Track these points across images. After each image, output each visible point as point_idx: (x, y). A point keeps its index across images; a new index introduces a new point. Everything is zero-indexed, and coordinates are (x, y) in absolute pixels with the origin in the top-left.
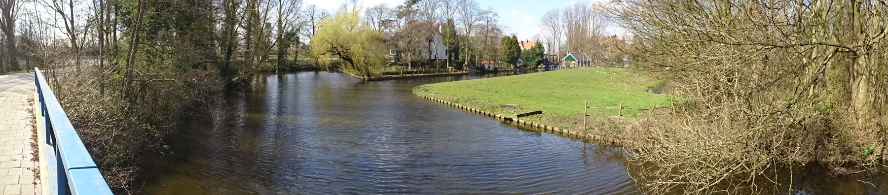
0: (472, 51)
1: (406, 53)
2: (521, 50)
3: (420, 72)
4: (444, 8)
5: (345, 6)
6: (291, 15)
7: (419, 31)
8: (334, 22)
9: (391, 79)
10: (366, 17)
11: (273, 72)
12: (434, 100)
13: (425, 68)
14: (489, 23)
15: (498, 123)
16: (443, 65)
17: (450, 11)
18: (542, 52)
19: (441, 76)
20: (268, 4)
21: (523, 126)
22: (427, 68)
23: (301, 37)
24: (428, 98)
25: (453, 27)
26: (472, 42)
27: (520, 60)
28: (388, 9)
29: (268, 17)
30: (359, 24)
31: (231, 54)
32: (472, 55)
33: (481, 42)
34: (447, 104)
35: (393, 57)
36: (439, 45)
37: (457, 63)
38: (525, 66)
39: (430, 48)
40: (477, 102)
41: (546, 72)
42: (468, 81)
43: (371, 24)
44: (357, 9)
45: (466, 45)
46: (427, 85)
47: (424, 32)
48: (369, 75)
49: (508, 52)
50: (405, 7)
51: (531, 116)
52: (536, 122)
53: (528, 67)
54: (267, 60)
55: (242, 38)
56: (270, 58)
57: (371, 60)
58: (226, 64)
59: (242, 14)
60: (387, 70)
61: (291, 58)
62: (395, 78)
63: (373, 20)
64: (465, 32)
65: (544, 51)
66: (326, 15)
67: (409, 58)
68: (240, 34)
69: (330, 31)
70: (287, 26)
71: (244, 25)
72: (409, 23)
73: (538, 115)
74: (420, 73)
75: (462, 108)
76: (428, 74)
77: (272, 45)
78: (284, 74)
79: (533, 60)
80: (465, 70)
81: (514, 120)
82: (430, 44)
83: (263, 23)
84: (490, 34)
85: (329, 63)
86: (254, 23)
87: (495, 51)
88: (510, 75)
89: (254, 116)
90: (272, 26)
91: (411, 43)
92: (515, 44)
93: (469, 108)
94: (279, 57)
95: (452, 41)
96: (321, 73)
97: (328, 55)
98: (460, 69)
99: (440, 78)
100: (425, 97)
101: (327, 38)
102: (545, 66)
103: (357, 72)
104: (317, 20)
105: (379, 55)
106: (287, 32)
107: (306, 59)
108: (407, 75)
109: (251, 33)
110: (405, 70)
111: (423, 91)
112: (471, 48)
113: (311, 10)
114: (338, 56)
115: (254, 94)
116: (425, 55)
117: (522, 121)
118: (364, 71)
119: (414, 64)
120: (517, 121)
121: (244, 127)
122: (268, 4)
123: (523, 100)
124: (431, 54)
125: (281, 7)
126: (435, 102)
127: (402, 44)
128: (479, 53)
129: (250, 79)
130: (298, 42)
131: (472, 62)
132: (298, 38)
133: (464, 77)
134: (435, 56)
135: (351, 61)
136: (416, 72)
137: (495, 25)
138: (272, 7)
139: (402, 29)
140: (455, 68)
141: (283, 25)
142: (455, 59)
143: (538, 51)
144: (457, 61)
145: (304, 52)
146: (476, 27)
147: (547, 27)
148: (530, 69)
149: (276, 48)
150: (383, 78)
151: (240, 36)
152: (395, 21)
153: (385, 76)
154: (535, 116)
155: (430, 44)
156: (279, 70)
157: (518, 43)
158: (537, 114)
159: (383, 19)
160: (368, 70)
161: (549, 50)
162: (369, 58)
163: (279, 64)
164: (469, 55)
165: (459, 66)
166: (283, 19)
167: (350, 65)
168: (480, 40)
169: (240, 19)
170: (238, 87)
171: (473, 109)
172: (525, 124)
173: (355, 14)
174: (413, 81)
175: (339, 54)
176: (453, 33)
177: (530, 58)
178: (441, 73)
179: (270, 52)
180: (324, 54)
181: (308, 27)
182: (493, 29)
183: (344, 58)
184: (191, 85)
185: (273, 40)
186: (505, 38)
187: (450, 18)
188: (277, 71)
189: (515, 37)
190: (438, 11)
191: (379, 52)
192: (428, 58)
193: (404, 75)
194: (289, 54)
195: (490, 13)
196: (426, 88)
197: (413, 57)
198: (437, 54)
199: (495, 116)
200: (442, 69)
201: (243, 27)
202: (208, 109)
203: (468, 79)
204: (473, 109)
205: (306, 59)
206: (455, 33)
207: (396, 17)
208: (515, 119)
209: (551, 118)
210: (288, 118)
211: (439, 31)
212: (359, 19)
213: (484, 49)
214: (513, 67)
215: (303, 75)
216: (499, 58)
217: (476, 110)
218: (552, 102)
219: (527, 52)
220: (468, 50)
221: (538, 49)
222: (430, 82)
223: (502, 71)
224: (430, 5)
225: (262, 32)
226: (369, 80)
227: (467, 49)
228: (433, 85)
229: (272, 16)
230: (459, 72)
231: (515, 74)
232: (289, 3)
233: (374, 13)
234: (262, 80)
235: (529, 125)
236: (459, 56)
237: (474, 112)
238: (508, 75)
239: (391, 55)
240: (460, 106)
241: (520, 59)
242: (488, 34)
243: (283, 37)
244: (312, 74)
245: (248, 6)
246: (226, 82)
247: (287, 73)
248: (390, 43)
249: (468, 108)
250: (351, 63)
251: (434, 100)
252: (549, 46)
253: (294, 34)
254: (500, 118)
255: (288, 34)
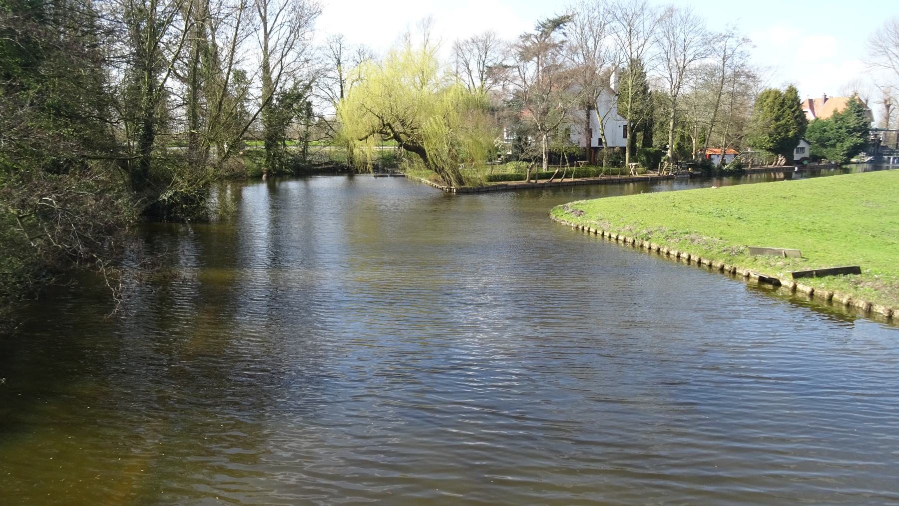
0: (683, 127)
1: (538, 133)
2: (807, 122)
3: (569, 174)
4: (622, 34)
5: (407, 37)
6: (291, 56)
7: (567, 87)
8: (387, 72)
9: (506, 189)
10: (455, 59)
11: (256, 178)
12: (596, 233)
13: (578, 165)
14: (728, 62)
15: (742, 287)
16: (617, 159)
17: (635, 40)
18: (866, 124)
19: (612, 182)
20: (237, 28)
21: (808, 299)
22: (581, 166)
23: (315, 101)
24: (583, 229)
25: (642, 75)
26: (684, 107)
27: (802, 144)
28: (499, 42)
29: (237, 57)
30: (438, 75)
31: (152, 140)
32: (682, 137)
33: (706, 105)
34: (625, 241)
35: (510, 144)
36: (609, 116)
37: (648, 154)
38: (815, 158)
39: (588, 123)
40: (693, 240)
41: (874, 173)
42: (672, 194)
43: (465, 76)
44: (433, 43)
45: (669, 114)
46: (580, 201)
47: (577, 88)
48: (460, 181)
49: (773, 126)
50: (536, 37)
51: (831, 277)
52: (843, 292)
53: (824, 162)
54: (241, 153)
55: (179, 103)
56: (247, 148)
57: (464, 151)
58: (142, 162)
59: (175, 49)
60: (498, 170)
61: (293, 148)
62: (515, 189)
63: (467, 65)
64: (668, 86)
65: (872, 120)
66: (367, 56)
67: (543, 144)
68: (174, 94)
69: (377, 89)
70: (283, 78)
71: (181, 75)
72: (544, 71)
73: (852, 275)
74: (566, 177)
75: (658, 250)
76: (585, 179)
77: (251, 118)
78: (281, 181)
79: (839, 144)
80: (668, 170)
81: (783, 283)
82: (588, 115)
83: (226, 71)
84: (727, 88)
85: (376, 157)
86: (205, 70)
87: (740, 124)
88: (775, 180)
89: (214, 274)
90: (248, 76)
91: (549, 114)
92: (791, 107)
93: (674, 253)
94: (268, 147)
95: (638, 106)
96: (363, 180)
97: (372, 140)
98: (654, 167)
99: (609, 186)
100: (577, 228)
101: (369, 104)
102: (869, 158)
103: (433, 175)
104: (348, 67)
105: (481, 140)
106: (284, 93)
107: (327, 149)
108: (540, 181)
109: (200, 93)
110: (535, 170)
111: (573, 215)
112: (681, 119)
113: (336, 46)
114: (394, 142)
115: (214, 227)
116: (578, 139)
117: (804, 287)
118: (450, 172)
119: (554, 158)
120: (791, 285)
121: (194, 300)
122: (237, 28)
123: (810, 240)
124: (591, 136)
125: (267, 36)
126: (599, 236)
127: (529, 116)
128: (700, 130)
129: (204, 194)
130: (310, 114)
131: (682, 152)
132: (309, 104)
133: (663, 185)
134: (600, 140)
135: (421, 152)
136: (559, 176)
137: (742, 65)
138: (247, 36)
139: (529, 83)
140: (644, 166)
141: (274, 76)
142: (644, 145)
143: (853, 122)
144: (648, 149)
145: (323, 135)
146: (695, 72)
147: (884, 59)
148: (828, 167)
149: (260, 127)
150: (488, 188)
151: (173, 97)
152: (513, 67)
153: (493, 184)
154: (841, 278)
155: (588, 115)
156: (269, 173)
157: (799, 104)
158: (845, 274)
159: (490, 64)
160: (458, 172)
161: (887, 118)
162: (460, 145)
163: (268, 160)
164: (677, 136)
165: (653, 161)
166: (272, 62)
167: (421, 160)
168: (704, 101)
169: (170, 58)
170: (176, 212)
171: (684, 255)
172: (812, 294)
173: (429, 55)
174: (551, 193)
175: (396, 137)
176: (642, 88)
177: (829, 139)
178: (613, 177)
179: (245, 135)
180: (366, 137)
181: (330, 82)
182: (737, 75)
183: (407, 147)
184: (46, 213)
185: (253, 108)
186: (768, 94)
187: (634, 56)
188: (264, 176)
189: (792, 90)
190: (608, 43)
191: (480, 133)
192: (585, 145)
193: (532, 181)
194: (290, 140)
195: (730, 39)
196: (580, 208)
197: (552, 143)
198: (603, 135)
199: (734, 273)
200: (615, 169)
201: (179, 77)
202: (95, 268)
203: (672, 189)
204: (684, 255)
205: (327, 149)
206: (646, 89)
207: (518, 58)
208: (787, 282)
209: (885, 286)
210: (295, 274)
211: (609, 86)
212: (437, 63)
213: (713, 121)
214: (784, 162)
215: (322, 183)
216: (749, 141)
217: (690, 256)
218: (889, 248)
219: (822, 126)
220: (675, 125)
221: (854, 115)
222: (588, 196)
223: (755, 171)
224: (591, 29)
225: (225, 90)
226: (460, 192)
227: (671, 123)
228: (595, 201)
229: (247, 55)
230: (652, 174)
231: (788, 176)
232: (285, 27)
233: (471, 51)
234: (232, 195)
235: (823, 299)
236: (654, 139)
237: (685, 261)
238: (769, 180)
239: (505, 140)
240: (654, 247)
241: (802, 142)
242: (725, 87)
243: (274, 102)
244: (340, 180)
245: (186, 30)
246: (144, 202)
247: (289, 180)
248: (505, 113)
249: (672, 252)
250: (421, 157)
251: (596, 233)
252: (888, 107)
253: (299, 96)
254: (748, 276)
255: (285, 96)
